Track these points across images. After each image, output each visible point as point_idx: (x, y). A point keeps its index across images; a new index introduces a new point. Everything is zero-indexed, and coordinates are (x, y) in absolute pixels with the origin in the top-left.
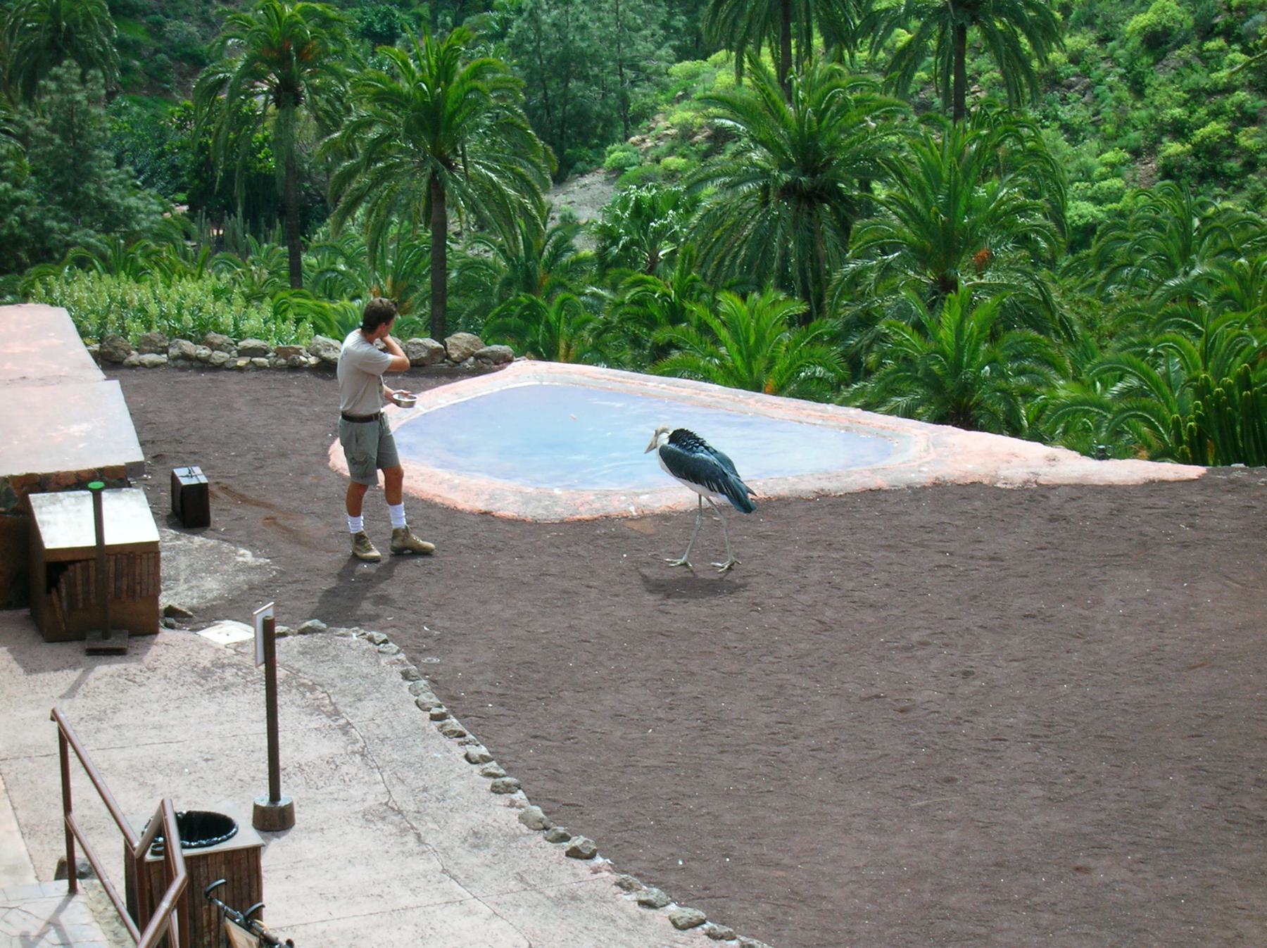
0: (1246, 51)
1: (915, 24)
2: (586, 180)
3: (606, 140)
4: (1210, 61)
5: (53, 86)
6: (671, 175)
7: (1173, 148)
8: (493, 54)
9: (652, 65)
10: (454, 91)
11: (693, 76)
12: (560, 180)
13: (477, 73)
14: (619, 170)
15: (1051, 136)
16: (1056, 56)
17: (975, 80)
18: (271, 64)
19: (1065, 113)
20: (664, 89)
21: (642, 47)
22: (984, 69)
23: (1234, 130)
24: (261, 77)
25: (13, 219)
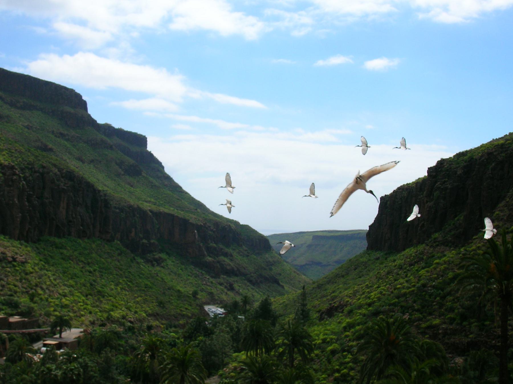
0: (351, 355)
1: (284, 347)
2: (214, 377)
3: (219, 369)
4: (345, 357)
5: (104, 352)
6: (232, 377)
7: (337, 375)
8: (196, 350)
9: (229, 354)
10: (187, 357)
11: (237, 356)
12: (209, 377)
13: (192, 354)
14: (221, 375)
15: (311, 371)
16: (312, 355)
17: (296, 359)
18: (150, 351)
19: (314, 367)
20: (231, 359)
21: (227, 350)
22: (298, 358)
23: (349, 371)
24: (147, 353)
25: (93, 380)
